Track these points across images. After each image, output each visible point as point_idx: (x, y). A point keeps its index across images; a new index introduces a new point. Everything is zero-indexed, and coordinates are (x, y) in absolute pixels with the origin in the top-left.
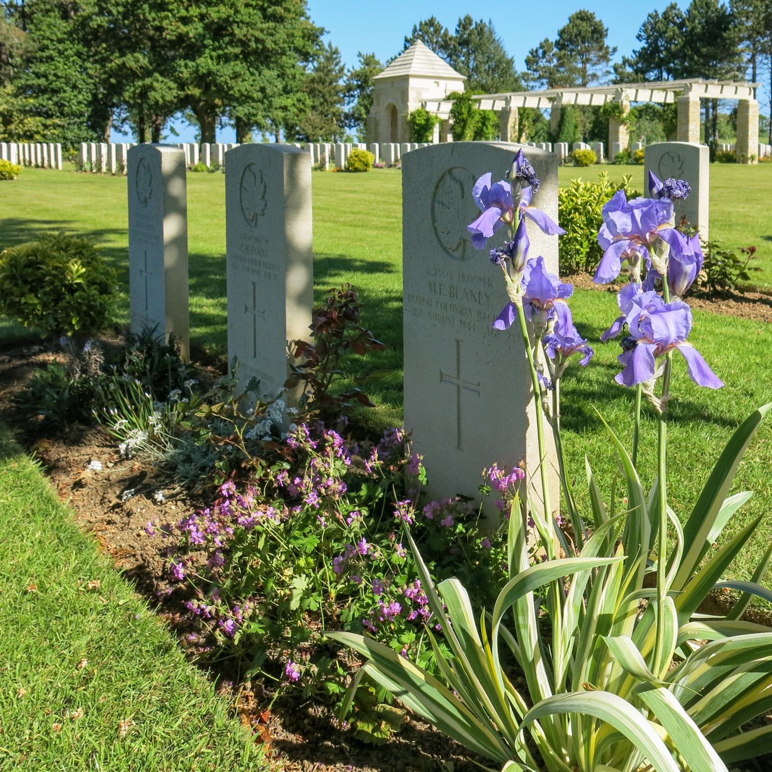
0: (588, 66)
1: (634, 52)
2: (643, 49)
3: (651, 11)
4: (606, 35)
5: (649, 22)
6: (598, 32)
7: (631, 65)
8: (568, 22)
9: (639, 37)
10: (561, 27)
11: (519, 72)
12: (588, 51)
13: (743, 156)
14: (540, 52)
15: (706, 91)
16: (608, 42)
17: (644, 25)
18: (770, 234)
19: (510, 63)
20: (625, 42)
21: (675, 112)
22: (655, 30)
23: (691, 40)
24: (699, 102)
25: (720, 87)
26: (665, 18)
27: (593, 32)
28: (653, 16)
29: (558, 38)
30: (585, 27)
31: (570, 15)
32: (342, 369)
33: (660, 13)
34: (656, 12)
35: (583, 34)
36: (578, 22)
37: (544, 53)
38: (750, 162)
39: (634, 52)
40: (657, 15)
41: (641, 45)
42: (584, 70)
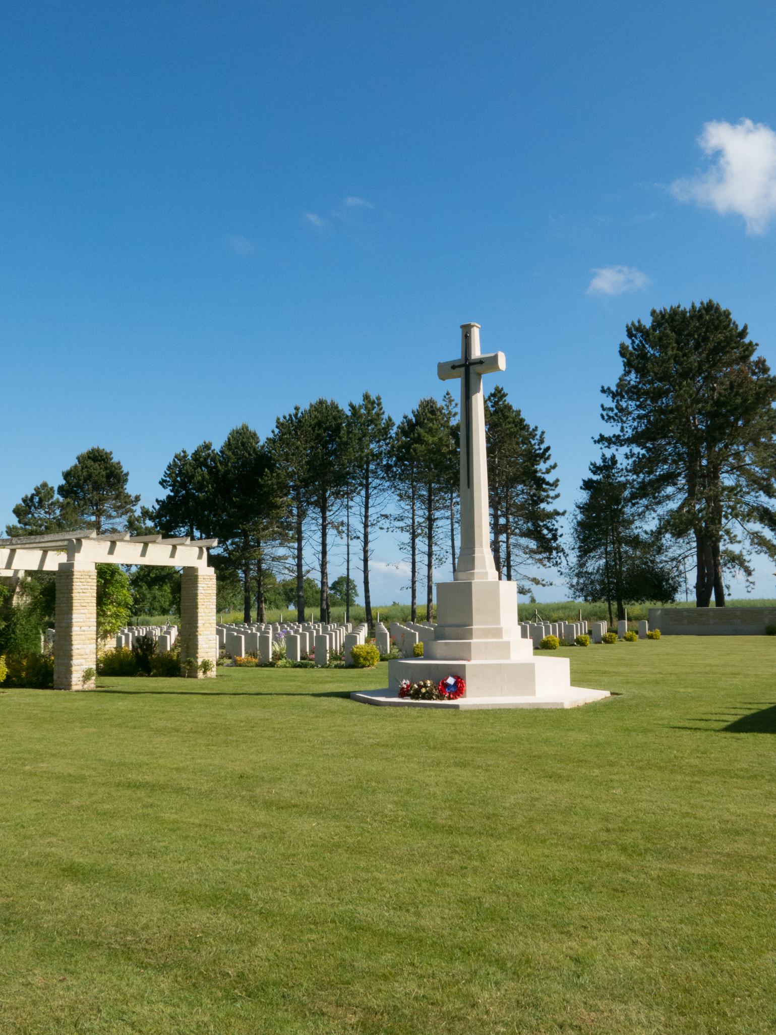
0: (103, 519)
1: (157, 501)
2: (169, 497)
3: (178, 451)
4: (126, 480)
5: (175, 464)
7: (152, 518)
8: (76, 462)
9: (163, 483)
10: (67, 467)
12: (102, 500)
13: (189, 663)
14: (37, 499)
15: (173, 555)
16: (130, 489)
17: (169, 467)
20: (148, 488)
22: (182, 474)
24: (94, 573)
25: (140, 546)
27: (108, 477)
28: (181, 457)
29: (63, 482)
30: (97, 469)
32: (630, 500)
33: (190, 452)
34: (184, 452)
35: (95, 478)
37: (41, 501)
38: (200, 675)
39: (157, 501)
40: (185, 456)
41: (165, 493)
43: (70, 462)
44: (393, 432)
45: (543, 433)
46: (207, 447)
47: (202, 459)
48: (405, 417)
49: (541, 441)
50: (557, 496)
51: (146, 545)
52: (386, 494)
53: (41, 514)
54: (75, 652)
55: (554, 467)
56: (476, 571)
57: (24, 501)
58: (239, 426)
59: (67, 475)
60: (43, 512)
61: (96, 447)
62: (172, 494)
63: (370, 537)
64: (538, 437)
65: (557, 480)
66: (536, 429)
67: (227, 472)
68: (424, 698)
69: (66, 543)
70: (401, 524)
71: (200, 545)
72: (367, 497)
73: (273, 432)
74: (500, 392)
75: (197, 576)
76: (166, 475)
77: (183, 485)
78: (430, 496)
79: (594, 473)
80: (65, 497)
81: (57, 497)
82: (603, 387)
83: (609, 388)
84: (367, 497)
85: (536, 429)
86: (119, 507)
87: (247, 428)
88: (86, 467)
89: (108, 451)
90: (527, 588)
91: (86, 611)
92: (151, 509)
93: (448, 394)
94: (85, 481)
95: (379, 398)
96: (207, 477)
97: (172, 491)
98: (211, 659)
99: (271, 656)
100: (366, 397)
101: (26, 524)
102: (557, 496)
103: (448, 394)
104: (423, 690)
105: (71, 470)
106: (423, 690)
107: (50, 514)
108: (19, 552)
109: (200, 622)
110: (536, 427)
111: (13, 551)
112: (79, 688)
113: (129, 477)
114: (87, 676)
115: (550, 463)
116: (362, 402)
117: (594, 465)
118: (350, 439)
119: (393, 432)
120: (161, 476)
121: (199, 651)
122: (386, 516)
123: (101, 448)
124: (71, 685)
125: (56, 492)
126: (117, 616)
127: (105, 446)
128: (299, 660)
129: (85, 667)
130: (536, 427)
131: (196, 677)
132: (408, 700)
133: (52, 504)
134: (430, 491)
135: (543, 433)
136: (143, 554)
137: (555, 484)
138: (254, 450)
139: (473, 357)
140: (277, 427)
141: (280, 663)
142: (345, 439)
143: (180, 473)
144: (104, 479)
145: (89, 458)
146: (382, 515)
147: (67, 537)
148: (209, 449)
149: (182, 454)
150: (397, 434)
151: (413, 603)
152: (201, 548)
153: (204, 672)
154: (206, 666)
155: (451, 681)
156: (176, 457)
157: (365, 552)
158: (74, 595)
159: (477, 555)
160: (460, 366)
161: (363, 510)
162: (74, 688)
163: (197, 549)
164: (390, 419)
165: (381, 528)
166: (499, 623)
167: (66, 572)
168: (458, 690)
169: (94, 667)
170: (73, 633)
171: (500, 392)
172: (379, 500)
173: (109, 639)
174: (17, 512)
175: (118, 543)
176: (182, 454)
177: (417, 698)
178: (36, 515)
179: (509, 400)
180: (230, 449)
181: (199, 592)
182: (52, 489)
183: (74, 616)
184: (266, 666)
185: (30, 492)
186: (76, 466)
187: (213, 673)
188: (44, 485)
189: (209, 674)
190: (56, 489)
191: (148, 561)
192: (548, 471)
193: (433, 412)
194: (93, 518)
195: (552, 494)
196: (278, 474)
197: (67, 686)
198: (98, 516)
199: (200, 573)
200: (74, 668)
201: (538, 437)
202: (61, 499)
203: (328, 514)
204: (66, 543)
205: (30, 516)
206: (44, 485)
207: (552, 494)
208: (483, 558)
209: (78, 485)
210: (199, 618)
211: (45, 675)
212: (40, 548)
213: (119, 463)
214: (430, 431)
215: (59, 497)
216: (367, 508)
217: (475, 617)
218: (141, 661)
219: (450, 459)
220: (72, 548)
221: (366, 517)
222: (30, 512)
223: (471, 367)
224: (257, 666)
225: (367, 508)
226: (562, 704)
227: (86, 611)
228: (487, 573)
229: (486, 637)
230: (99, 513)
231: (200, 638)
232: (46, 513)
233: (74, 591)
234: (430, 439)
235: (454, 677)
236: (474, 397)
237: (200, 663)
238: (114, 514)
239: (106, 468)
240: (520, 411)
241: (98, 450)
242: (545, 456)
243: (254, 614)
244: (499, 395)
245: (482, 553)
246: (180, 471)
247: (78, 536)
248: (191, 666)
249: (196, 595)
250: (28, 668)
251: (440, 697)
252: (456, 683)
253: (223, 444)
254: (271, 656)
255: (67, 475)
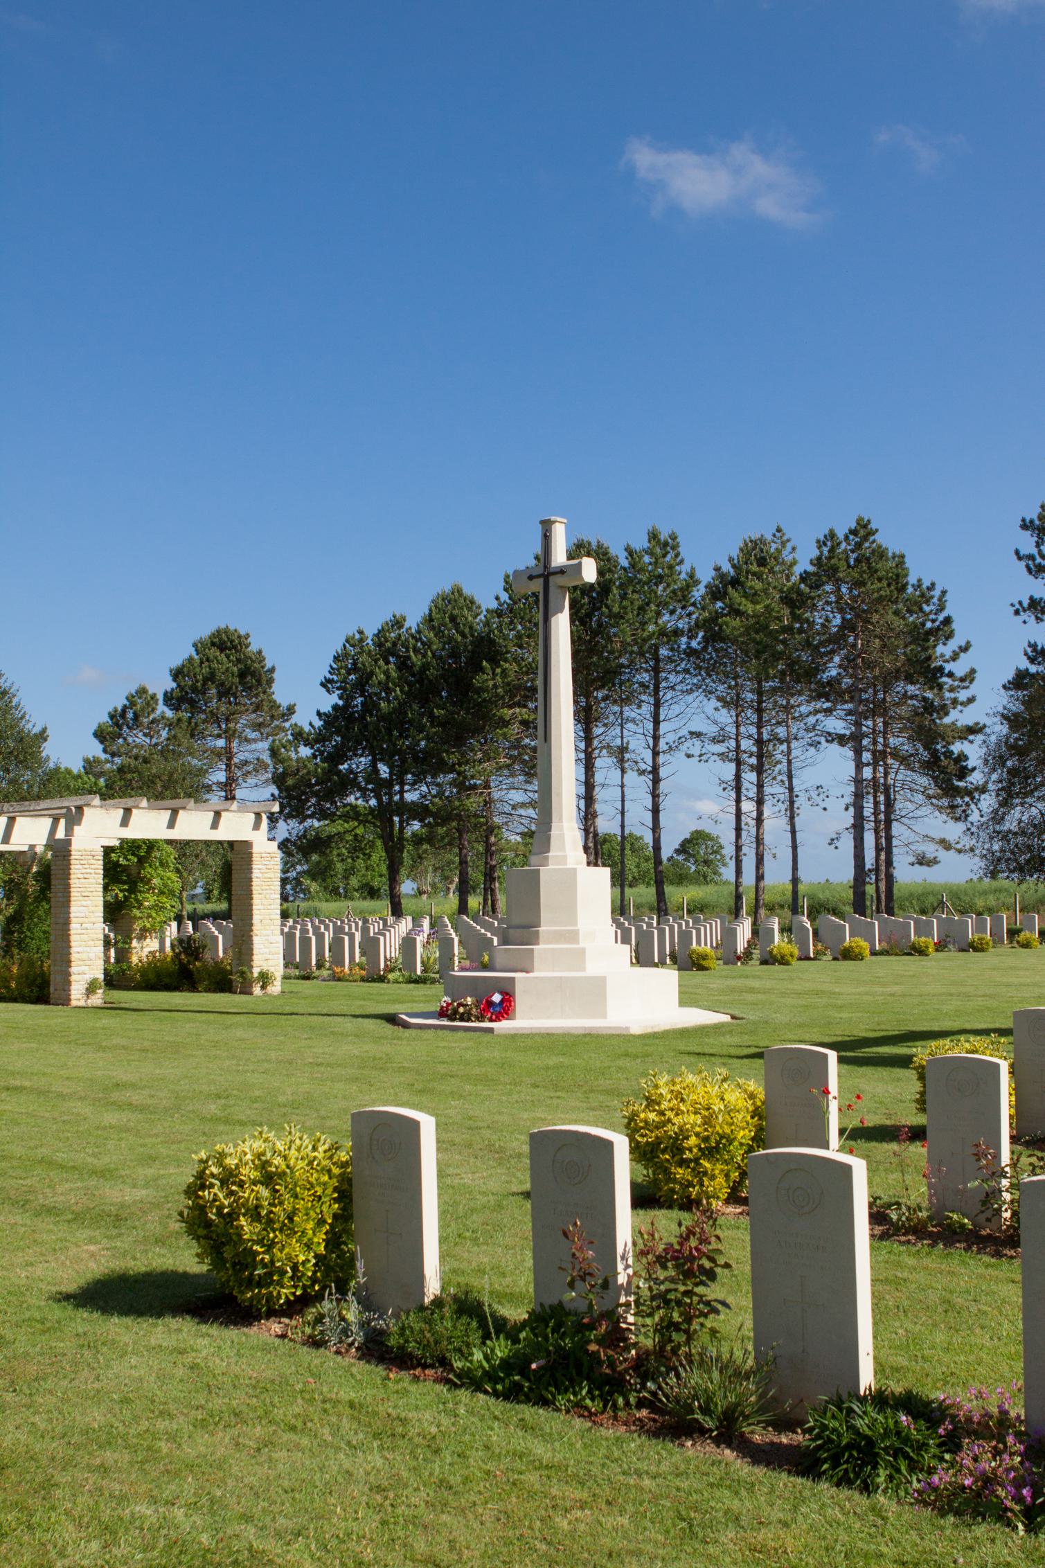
1: (319, 714)
2: (335, 707)
3: (352, 631)
4: (270, 681)
6: (253, 674)
9: (326, 684)
10: (177, 662)
11: (1005, 701)
13: (242, 973)
14: (130, 715)
16: (281, 693)
18: (1040, 1133)
19: (302, 729)
21: (45, 876)
22: (351, 672)
23: (421, 687)
24: (100, 854)
26: (380, 645)
27: (242, 675)
28: (355, 642)
30: (224, 664)
31: (197, 638)
33: (370, 632)
34: (361, 632)
36: (214, 652)
38: (257, 990)
39: (319, 714)
41: (328, 702)
42: (228, 754)
43: (182, 652)
44: (698, 593)
45: (944, 593)
46: (398, 623)
47: (388, 645)
48: (717, 569)
49: (941, 608)
50: (971, 700)
51: (175, 812)
52: (690, 698)
53: (138, 738)
54: (74, 957)
55: (965, 648)
56: (550, 854)
57: (112, 717)
58: (448, 589)
59: (177, 674)
60: (140, 734)
61: (223, 626)
62: (341, 703)
63: (663, 772)
64: (935, 600)
65: (973, 671)
66: (932, 586)
67: (425, 667)
68: (462, 1020)
69: (64, 811)
70: (720, 748)
71: (257, 810)
72: (657, 705)
73: (497, 598)
74: (865, 526)
75: (251, 853)
76: (332, 671)
77: (361, 686)
78: (760, 702)
79: (1032, 660)
80: (176, 708)
81: (161, 708)
82: (1024, 520)
83: (1032, 522)
84: (657, 705)
85: (932, 586)
86: (260, 725)
87: (460, 591)
88: (208, 660)
89: (243, 633)
90: (930, 856)
91: (89, 903)
92: (307, 728)
93: (779, 530)
94: (205, 680)
95: (673, 537)
96: (394, 674)
97: (340, 698)
98: (272, 969)
99: (382, 966)
100: (653, 536)
101: (113, 755)
102: (971, 700)
103: (779, 530)
104: (461, 1010)
105: (183, 666)
106: (461, 1010)
107: (152, 737)
108: (20, 821)
109: (255, 917)
110: (933, 584)
111: (12, 821)
112: (82, 1003)
113: (275, 675)
114: (91, 989)
115: (953, 645)
116: (646, 545)
117: (1033, 646)
118: (625, 608)
119: (698, 593)
120: (324, 672)
121: (255, 957)
122: (697, 735)
123: (232, 628)
124: (70, 1000)
125: (161, 702)
126: (159, 908)
127: (240, 626)
128: (419, 973)
129: (88, 977)
130: (933, 584)
131: (251, 994)
132: (445, 1022)
133: (152, 722)
134: (760, 693)
135: (944, 593)
136: (171, 825)
137: (970, 677)
138: (471, 628)
139: (554, 564)
140: (506, 590)
141: (391, 976)
142: (616, 609)
143: (355, 669)
144: (237, 680)
145: (213, 644)
146: (692, 733)
147: (66, 804)
148: (401, 627)
149: (357, 636)
150: (703, 598)
151: (795, 881)
152: (258, 815)
153: (263, 987)
154: (265, 979)
155: (497, 998)
156: (347, 641)
157: (655, 795)
158: (72, 881)
159: (554, 832)
160: (538, 576)
161: (650, 726)
162: (74, 1003)
163: (253, 816)
164: (691, 575)
165: (689, 756)
166: (576, 924)
167: (61, 850)
168: (505, 1010)
169: (101, 977)
170: (72, 932)
171: (865, 526)
172: (676, 709)
173: (148, 940)
174: (100, 735)
175: (134, 811)
176: (357, 636)
177: (453, 1020)
178: (130, 740)
179: (881, 539)
180: (433, 628)
181: (254, 875)
182: (153, 697)
183: (73, 909)
184: (374, 981)
185: (120, 702)
186: (191, 659)
187: (276, 988)
188: (142, 691)
189: (270, 989)
190: (160, 697)
191: (176, 834)
192: (955, 657)
193: (762, 562)
194: (221, 743)
195: (963, 695)
196: (504, 671)
197: (66, 1001)
198: (229, 740)
199: (255, 849)
200: (73, 978)
201: (935, 600)
202: (169, 714)
203: (598, 730)
204: (64, 811)
205: (121, 741)
206: (142, 691)
207: (963, 695)
208: (562, 836)
209: (194, 689)
210: (255, 912)
211: (42, 988)
212: (50, 816)
213: (260, 652)
214: (753, 597)
215: (166, 709)
216: (657, 722)
217: (545, 915)
218: (186, 972)
219: (784, 642)
220: (74, 818)
221: (656, 738)
222: (120, 736)
223: (551, 578)
224: (363, 980)
225: (657, 722)
226: (627, 1028)
227: (89, 903)
228: (566, 856)
229: (557, 942)
230: (229, 735)
231: (256, 940)
232: (145, 735)
233: (72, 876)
234: (749, 608)
235: (501, 993)
236: (553, 620)
237: (256, 975)
238: (253, 735)
239: (239, 661)
240: (903, 556)
241: (226, 631)
242: (945, 629)
243: (474, 902)
244: (862, 532)
245: (562, 829)
246: (355, 664)
247: (79, 803)
248: (245, 979)
249: (250, 880)
250: (20, 977)
251: (480, 1018)
252: (502, 1001)
253: (419, 619)
254: (382, 966)
255: (177, 674)
